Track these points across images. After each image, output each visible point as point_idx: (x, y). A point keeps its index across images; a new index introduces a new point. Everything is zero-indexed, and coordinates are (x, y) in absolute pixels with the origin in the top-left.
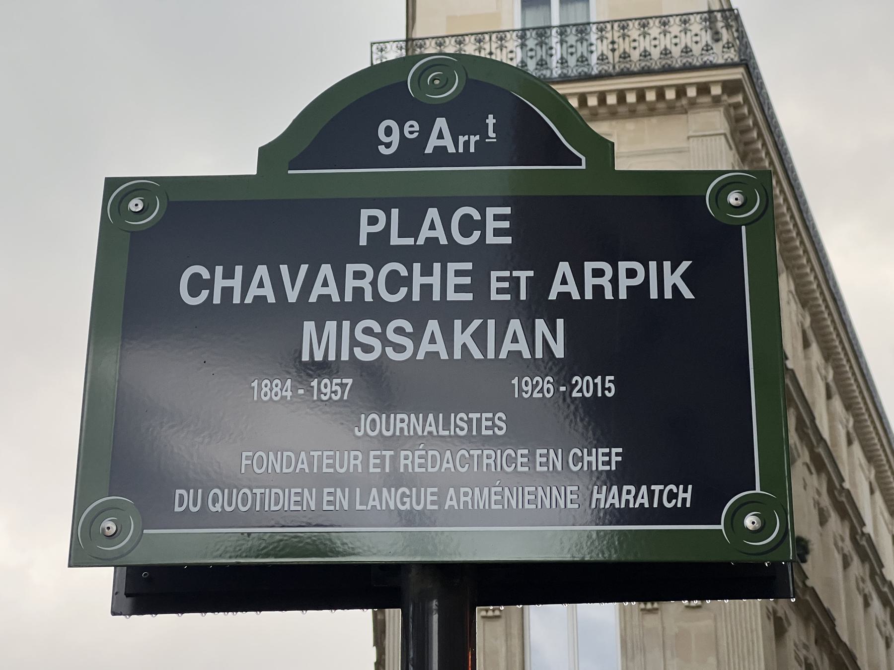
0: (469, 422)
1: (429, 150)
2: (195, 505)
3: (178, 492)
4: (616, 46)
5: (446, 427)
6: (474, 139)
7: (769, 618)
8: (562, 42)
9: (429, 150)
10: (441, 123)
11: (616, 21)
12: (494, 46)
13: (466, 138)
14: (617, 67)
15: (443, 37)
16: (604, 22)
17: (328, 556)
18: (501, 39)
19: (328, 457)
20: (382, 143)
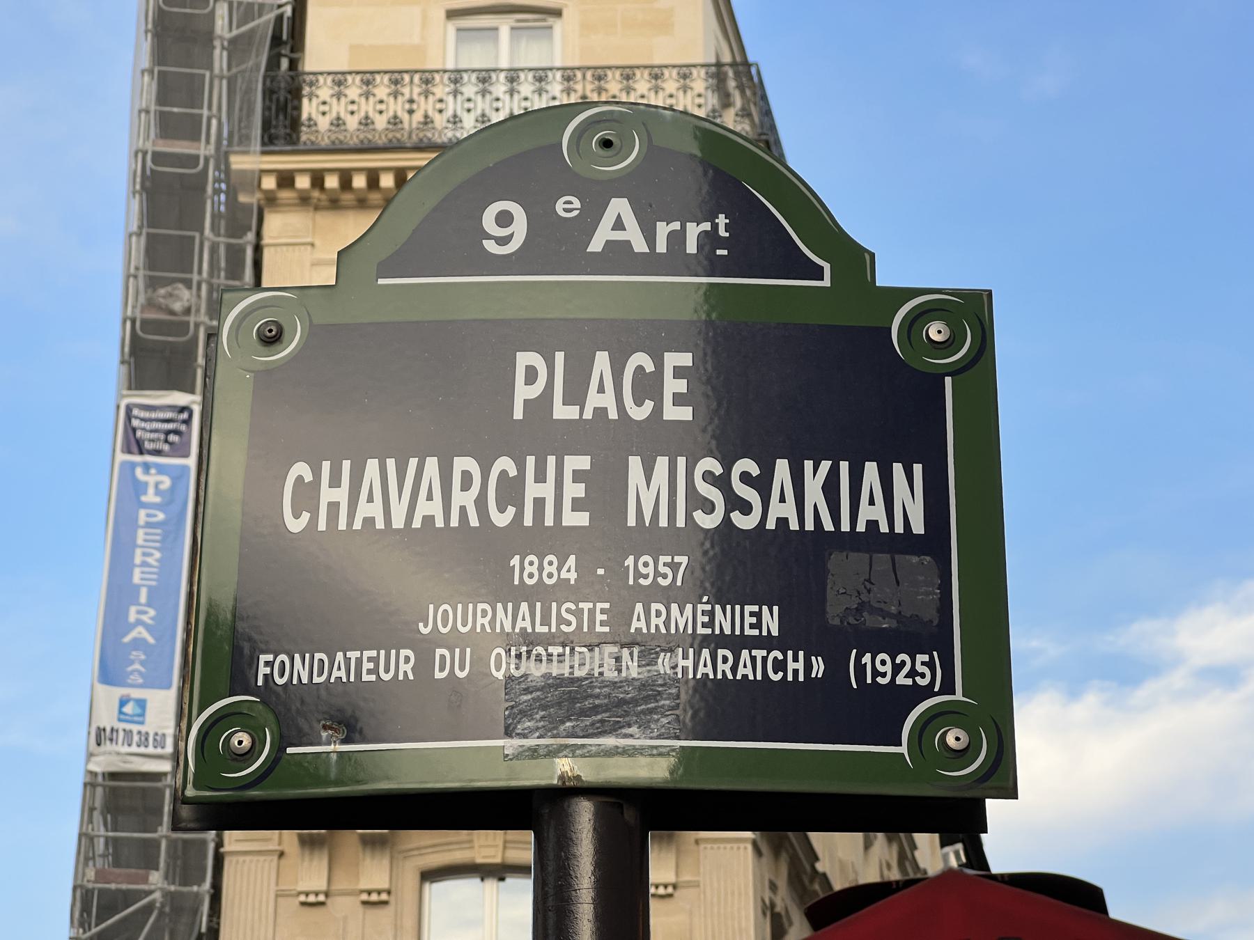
0: (578, 613)
1: (596, 245)
2: (462, 668)
3: (439, 652)
4: (407, 106)
5: (546, 621)
6: (693, 231)
7: (764, 914)
8: (512, 92)
9: (596, 245)
10: (619, 207)
11: (589, 68)
12: (416, 90)
13: (676, 226)
14: (414, 137)
15: (343, 73)
16: (572, 69)
17: (347, 785)
18: (427, 82)
19: (370, 659)
20: (490, 237)
